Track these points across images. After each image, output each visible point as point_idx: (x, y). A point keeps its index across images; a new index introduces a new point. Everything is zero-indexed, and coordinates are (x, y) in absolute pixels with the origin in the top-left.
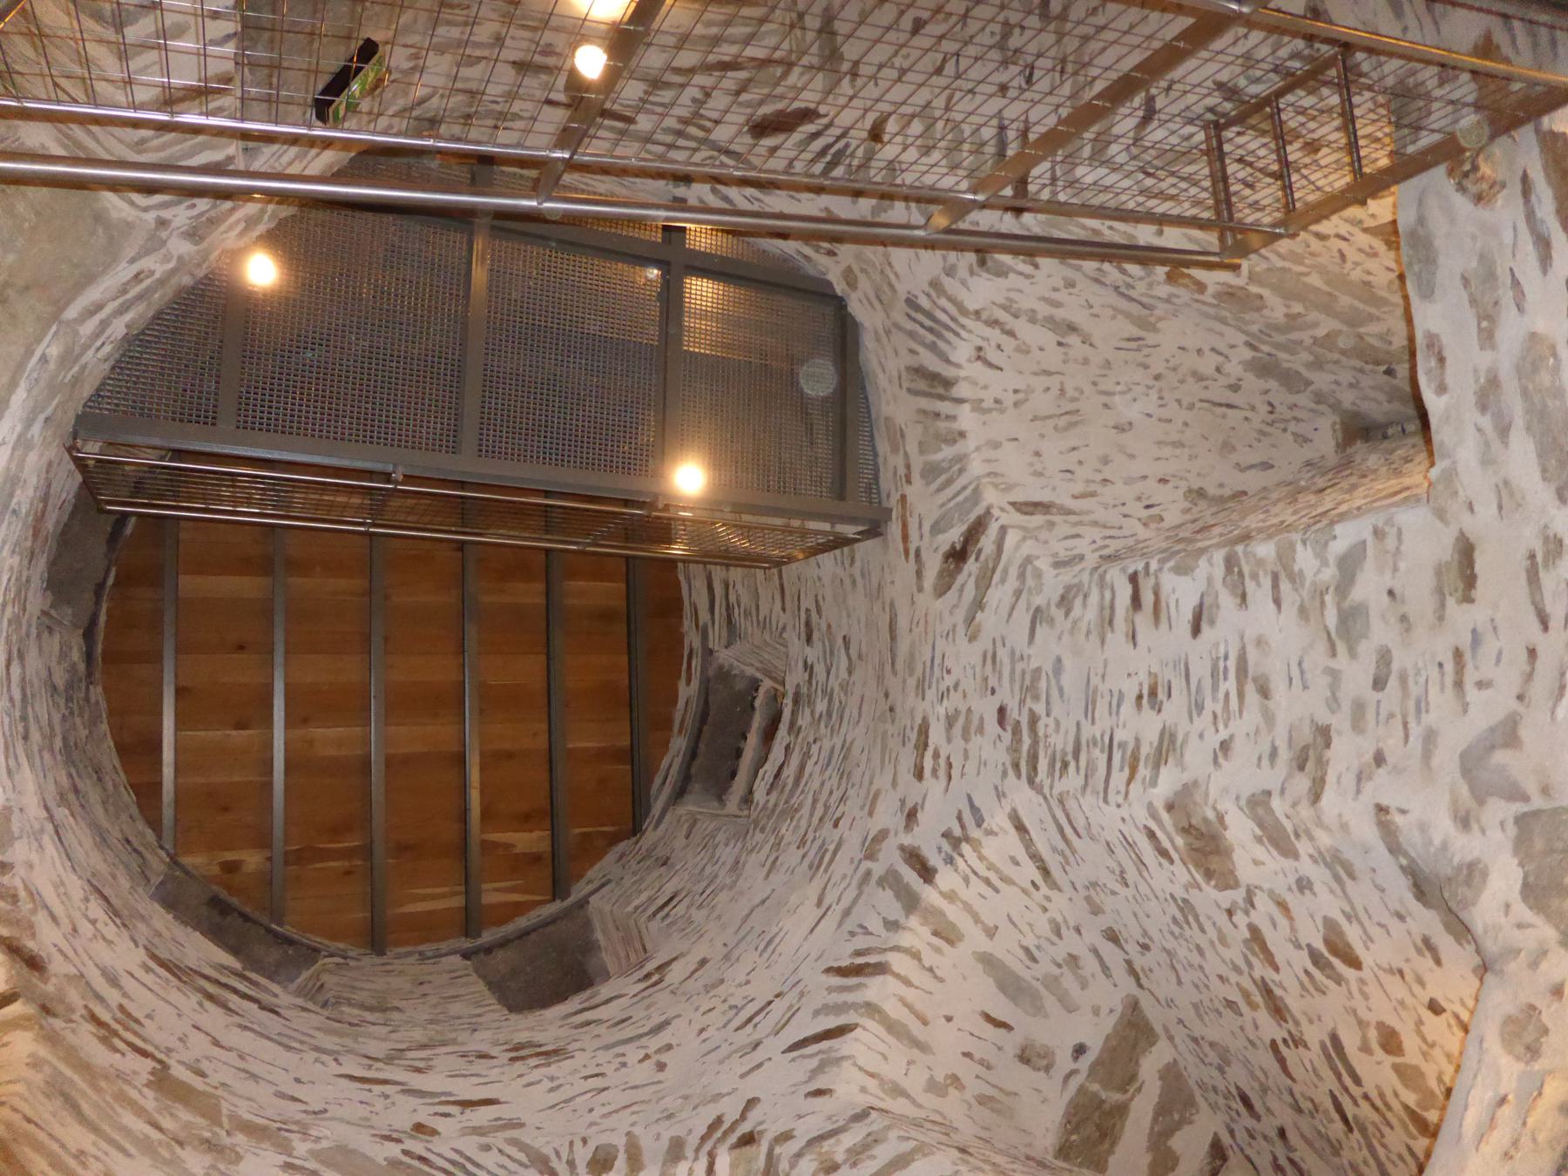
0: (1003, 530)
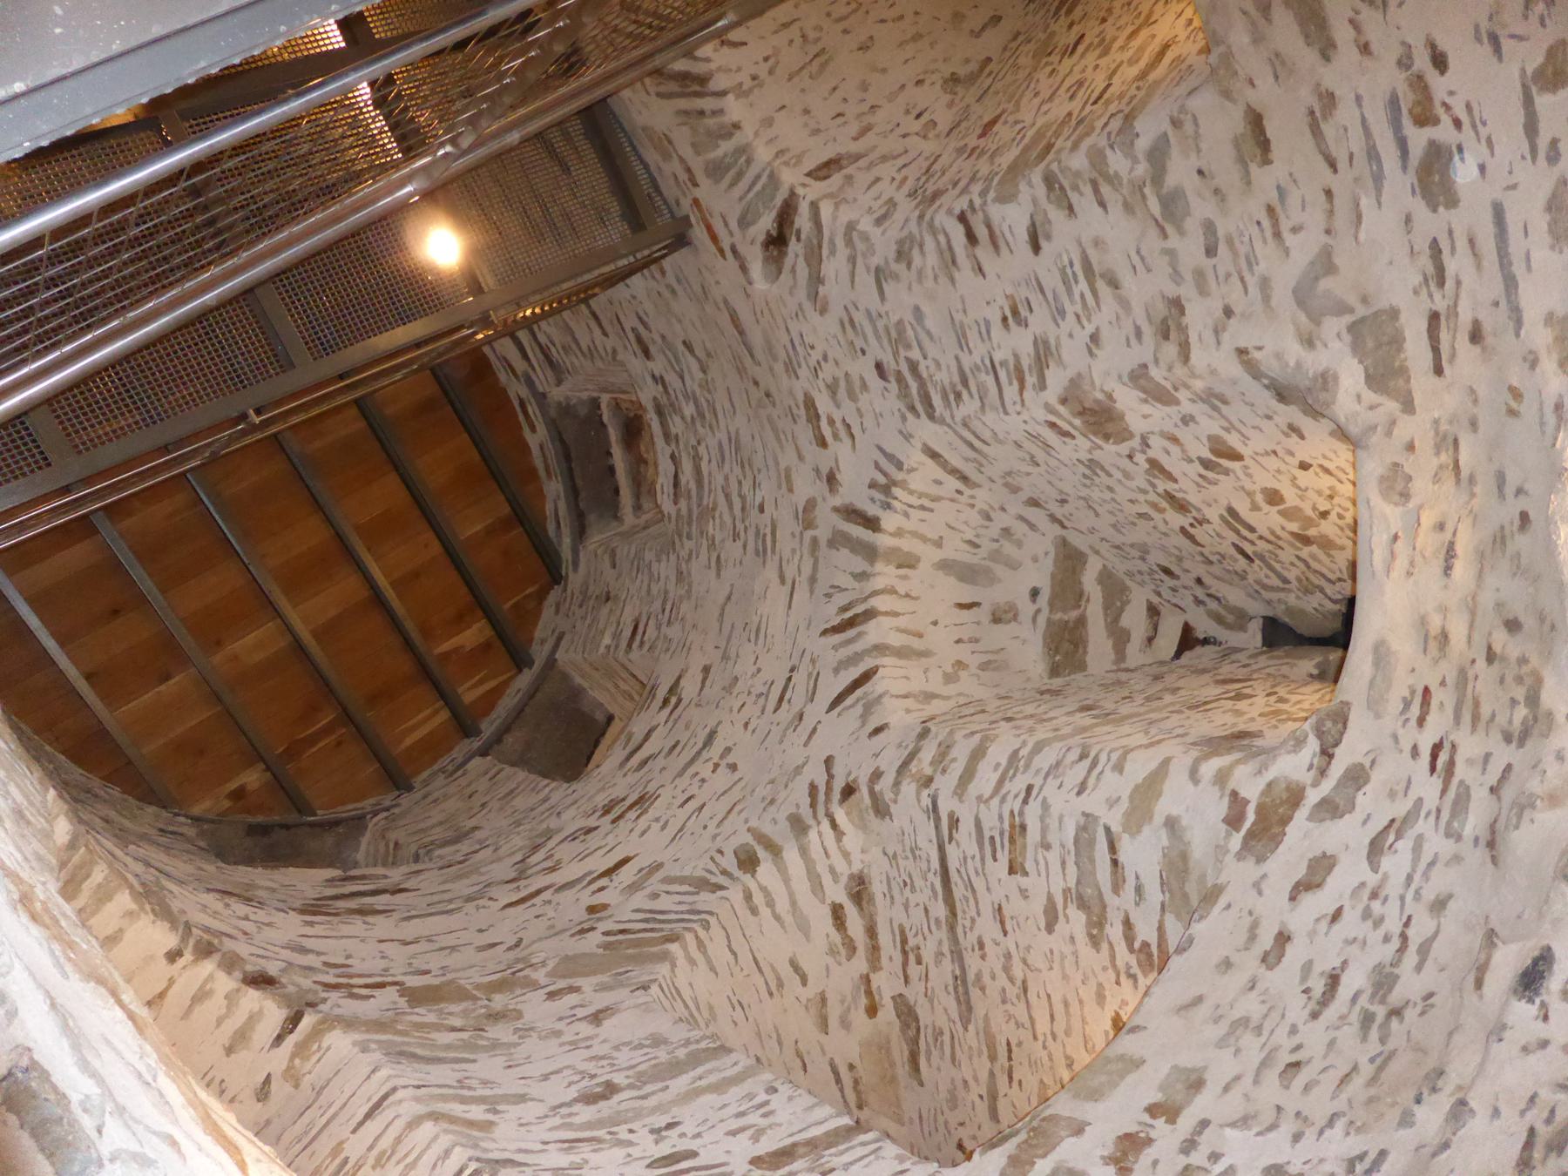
0: (814, 206)
